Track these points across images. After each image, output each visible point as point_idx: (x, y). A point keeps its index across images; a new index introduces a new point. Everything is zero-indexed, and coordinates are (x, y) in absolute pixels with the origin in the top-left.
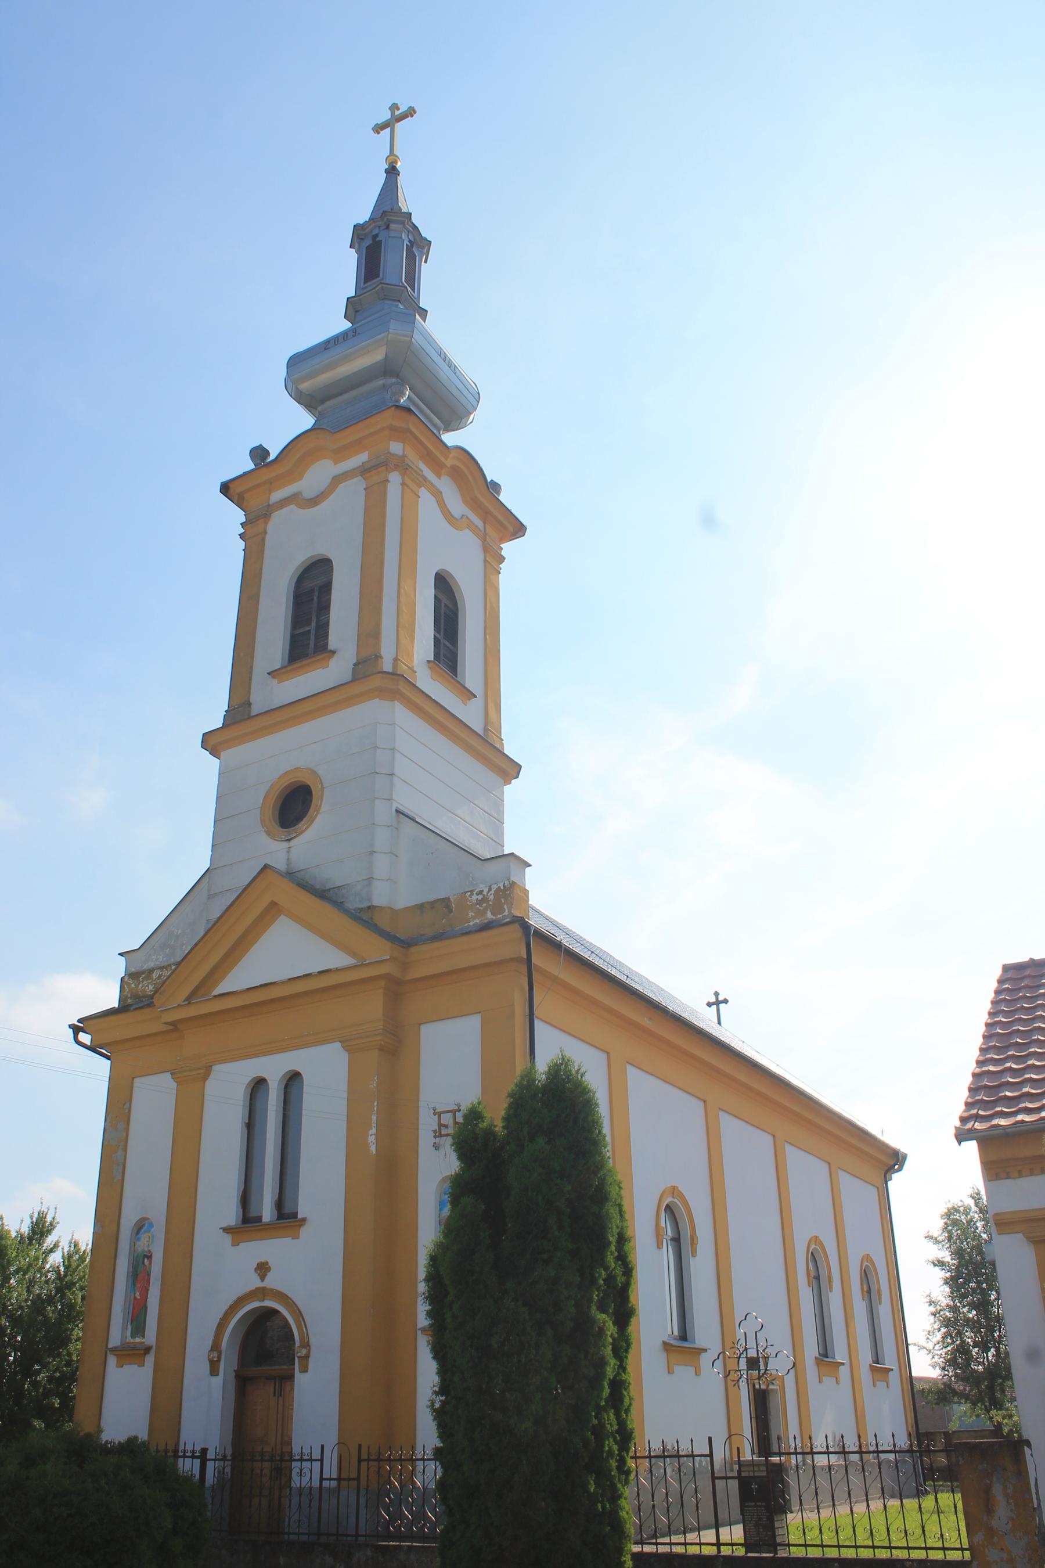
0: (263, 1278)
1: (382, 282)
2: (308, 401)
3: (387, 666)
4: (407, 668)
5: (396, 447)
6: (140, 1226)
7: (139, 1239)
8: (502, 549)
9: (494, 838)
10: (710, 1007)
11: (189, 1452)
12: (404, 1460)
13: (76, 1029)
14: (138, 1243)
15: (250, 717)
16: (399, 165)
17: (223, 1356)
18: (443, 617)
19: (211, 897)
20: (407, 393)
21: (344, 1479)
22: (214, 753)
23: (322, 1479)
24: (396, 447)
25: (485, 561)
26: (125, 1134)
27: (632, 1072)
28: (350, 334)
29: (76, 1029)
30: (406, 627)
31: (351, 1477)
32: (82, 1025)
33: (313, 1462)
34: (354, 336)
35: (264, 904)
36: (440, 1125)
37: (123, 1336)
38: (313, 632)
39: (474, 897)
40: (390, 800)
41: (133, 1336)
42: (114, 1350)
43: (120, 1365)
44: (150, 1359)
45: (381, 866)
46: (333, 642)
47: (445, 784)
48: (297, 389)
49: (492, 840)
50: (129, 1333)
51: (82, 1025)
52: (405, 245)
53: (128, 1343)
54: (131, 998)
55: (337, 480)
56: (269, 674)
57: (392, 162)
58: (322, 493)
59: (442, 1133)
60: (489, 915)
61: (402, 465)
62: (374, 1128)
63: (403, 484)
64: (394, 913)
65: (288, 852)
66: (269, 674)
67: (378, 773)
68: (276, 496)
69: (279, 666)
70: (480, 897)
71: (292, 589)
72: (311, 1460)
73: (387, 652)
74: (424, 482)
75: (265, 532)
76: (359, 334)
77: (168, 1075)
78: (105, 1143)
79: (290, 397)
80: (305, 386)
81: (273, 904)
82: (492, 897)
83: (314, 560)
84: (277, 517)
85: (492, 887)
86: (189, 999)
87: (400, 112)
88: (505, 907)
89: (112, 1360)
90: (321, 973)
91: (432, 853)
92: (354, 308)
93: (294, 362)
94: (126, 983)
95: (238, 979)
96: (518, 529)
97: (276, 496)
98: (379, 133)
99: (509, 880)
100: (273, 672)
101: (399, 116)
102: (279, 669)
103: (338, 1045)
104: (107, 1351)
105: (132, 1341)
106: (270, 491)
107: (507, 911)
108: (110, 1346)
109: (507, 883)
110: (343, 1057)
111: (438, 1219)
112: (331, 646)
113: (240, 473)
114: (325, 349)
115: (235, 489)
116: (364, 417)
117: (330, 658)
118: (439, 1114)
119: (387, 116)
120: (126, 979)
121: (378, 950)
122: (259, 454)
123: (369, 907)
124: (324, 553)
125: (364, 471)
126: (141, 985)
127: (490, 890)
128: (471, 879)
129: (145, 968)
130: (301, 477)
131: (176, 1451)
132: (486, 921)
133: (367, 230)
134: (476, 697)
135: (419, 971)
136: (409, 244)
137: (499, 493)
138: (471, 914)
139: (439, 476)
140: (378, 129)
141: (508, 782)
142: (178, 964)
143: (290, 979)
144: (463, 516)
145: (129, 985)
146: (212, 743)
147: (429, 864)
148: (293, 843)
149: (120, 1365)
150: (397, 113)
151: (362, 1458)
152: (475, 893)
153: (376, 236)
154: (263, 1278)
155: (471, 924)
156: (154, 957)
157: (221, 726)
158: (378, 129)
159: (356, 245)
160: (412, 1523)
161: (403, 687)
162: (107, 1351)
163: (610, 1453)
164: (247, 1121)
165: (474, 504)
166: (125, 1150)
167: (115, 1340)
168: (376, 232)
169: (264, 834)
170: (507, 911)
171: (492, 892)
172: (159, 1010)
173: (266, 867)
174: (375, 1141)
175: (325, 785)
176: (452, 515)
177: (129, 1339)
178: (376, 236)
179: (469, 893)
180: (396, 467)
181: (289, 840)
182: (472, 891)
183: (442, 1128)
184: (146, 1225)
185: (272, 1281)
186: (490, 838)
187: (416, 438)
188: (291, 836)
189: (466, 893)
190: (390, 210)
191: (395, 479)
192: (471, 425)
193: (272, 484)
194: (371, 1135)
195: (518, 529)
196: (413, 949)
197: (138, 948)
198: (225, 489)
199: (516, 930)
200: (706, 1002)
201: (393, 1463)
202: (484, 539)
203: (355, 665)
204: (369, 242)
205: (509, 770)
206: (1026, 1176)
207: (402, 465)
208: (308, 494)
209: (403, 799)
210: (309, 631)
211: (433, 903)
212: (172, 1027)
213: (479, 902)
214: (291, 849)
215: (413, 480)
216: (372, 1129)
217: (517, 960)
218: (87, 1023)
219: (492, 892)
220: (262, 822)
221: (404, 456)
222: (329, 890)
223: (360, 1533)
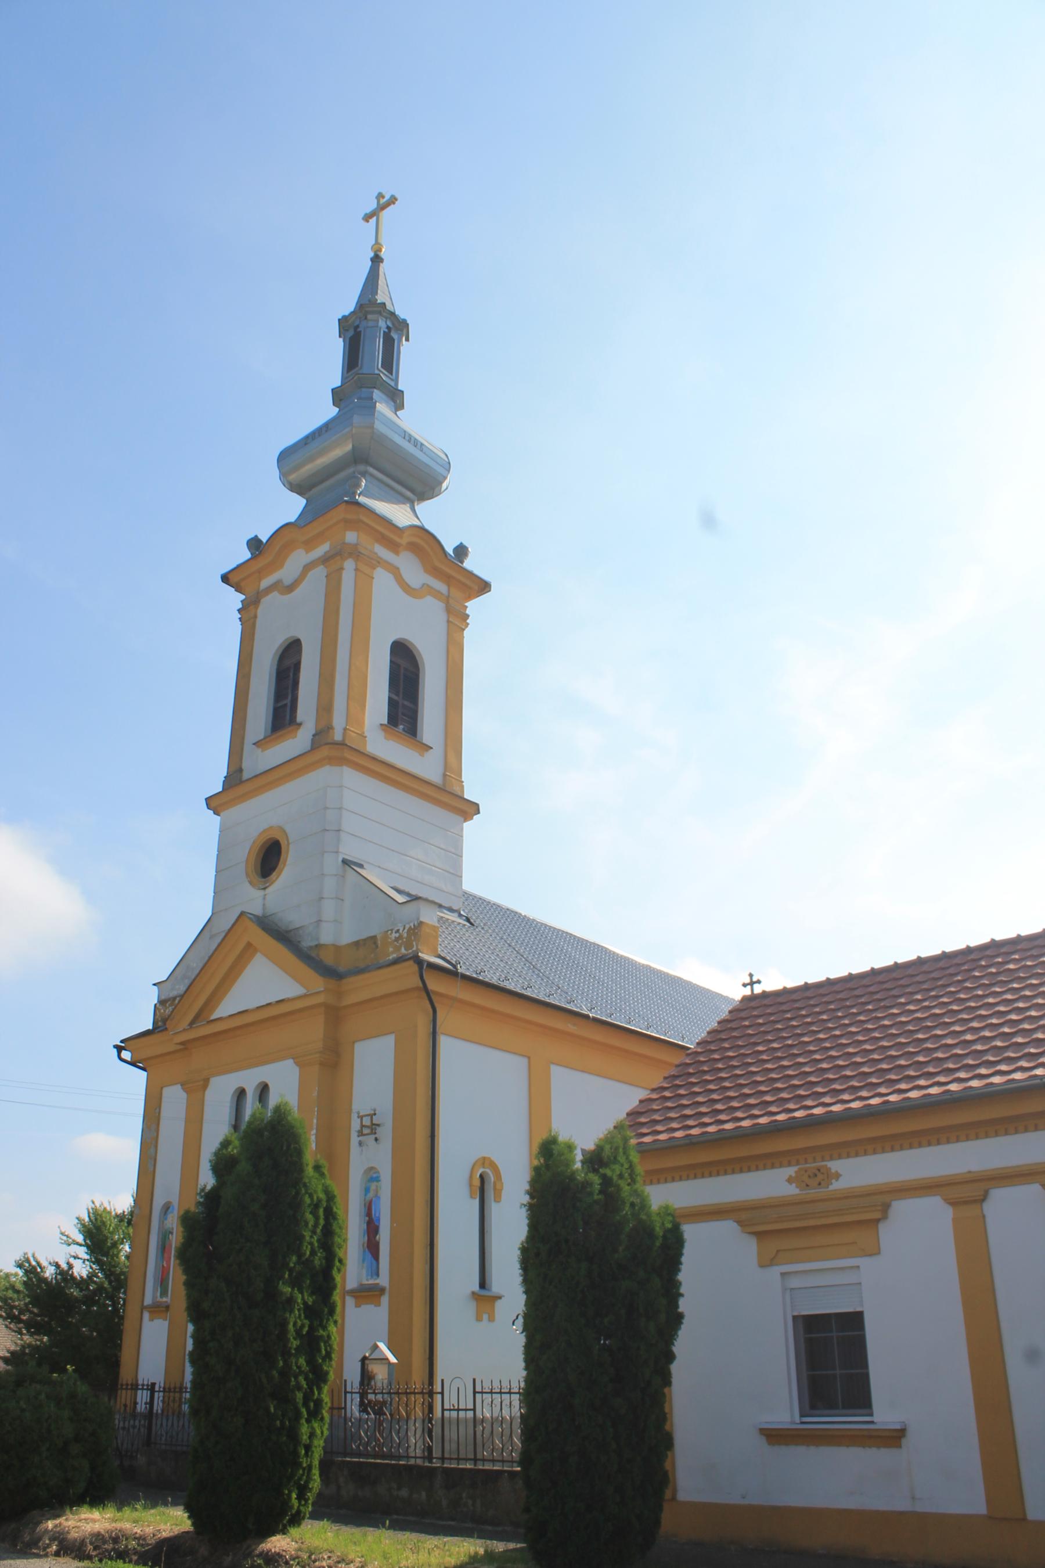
1: (360, 372)
2: (297, 488)
3: (338, 736)
4: (355, 735)
5: (351, 537)
6: (167, 1208)
7: (166, 1219)
8: (466, 607)
9: (451, 871)
12: (401, 1393)
13: (119, 1049)
14: (165, 1222)
15: (241, 782)
16: (382, 254)
18: (402, 677)
19: (212, 937)
20: (363, 484)
21: (335, 1409)
22: (216, 813)
23: (443, 1410)
24: (351, 537)
25: (448, 621)
26: (155, 1134)
27: (556, 1071)
28: (317, 435)
29: (119, 1049)
30: (358, 697)
31: (468, 1407)
32: (123, 1045)
34: (326, 431)
35: (241, 946)
36: (362, 1126)
37: (154, 1297)
38: (289, 704)
39: (394, 935)
40: (337, 852)
41: (161, 1296)
42: (147, 1307)
43: (358, 1305)
44: (385, 1300)
45: (328, 909)
46: (300, 716)
48: (288, 481)
49: (448, 872)
50: (159, 1294)
51: (123, 1045)
52: (382, 332)
53: (158, 1302)
55: (307, 568)
56: (254, 744)
57: (377, 251)
58: (295, 581)
59: (364, 1133)
60: (403, 951)
61: (354, 552)
63: (356, 570)
64: (337, 948)
65: (264, 899)
66: (254, 744)
67: (328, 830)
68: (265, 583)
69: (262, 737)
71: (275, 667)
73: (338, 722)
74: (380, 562)
75: (255, 617)
77: (179, 1086)
78: (143, 1141)
79: (283, 487)
80: (293, 477)
81: (249, 945)
82: (405, 935)
83: (290, 641)
84: (265, 601)
86: (191, 1024)
87: (385, 200)
88: (414, 943)
89: (146, 1315)
90: (278, 1002)
92: (338, 396)
93: (284, 456)
94: (158, 1008)
95: (226, 1008)
96: (484, 587)
97: (265, 583)
98: (368, 221)
99: (418, 919)
100: (258, 742)
101: (384, 203)
103: (290, 1062)
104: (143, 1308)
105: (161, 1300)
106: (260, 580)
107: (415, 947)
108: (146, 1303)
109: (416, 923)
110: (296, 1070)
111: (363, 1203)
112: (299, 719)
113: (234, 565)
114: (306, 444)
115: (234, 579)
116: (335, 506)
117: (298, 729)
119: (373, 205)
120: (158, 1005)
121: (319, 983)
123: (316, 946)
124: (293, 635)
125: (325, 560)
127: (404, 929)
128: (392, 919)
130: (282, 566)
131: (181, 1388)
132: (401, 955)
133: (350, 322)
134: (432, 748)
135: (350, 999)
136: (386, 330)
138: (391, 949)
139: (397, 553)
140: (367, 218)
141: (466, 820)
142: (182, 996)
143: (258, 1008)
144: (424, 584)
146: (214, 803)
148: (268, 890)
150: (382, 201)
151: (477, 1390)
152: (394, 931)
153: (358, 326)
155: (391, 958)
157: (221, 790)
158: (367, 218)
159: (342, 336)
160: (368, 1444)
161: (348, 755)
162: (143, 1308)
163: (299, 1387)
164: (233, 1123)
165: (435, 571)
166: (156, 1147)
167: (148, 1301)
168: (357, 323)
169: (247, 884)
170: (415, 947)
171: (406, 931)
172: (171, 1033)
173: (242, 914)
175: (290, 841)
176: (409, 586)
177: (159, 1299)
178: (358, 326)
179: (390, 932)
180: (350, 555)
181: (264, 889)
182: (392, 930)
183: (364, 1128)
186: (445, 871)
187: (367, 525)
189: (388, 931)
190: (367, 302)
191: (349, 565)
192: (446, 491)
193: (261, 573)
195: (484, 587)
196: (345, 981)
197: (165, 979)
198: (225, 579)
199: (412, 967)
201: (401, 1396)
202: (447, 600)
203: (314, 736)
204: (351, 333)
205: (469, 810)
206: (954, 1143)
207: (354, 552)
208: (287, 582)
209: (350, 850)
210: (286, 705)
211: (364, 940)
212: (181, 1047)
213: (397, 939)
214: (266, 896)
215: (368, 563)
217: (417, 989)
218: (127, 1043)
220: (247, 875)
221: (357, 545)
222: (291, 931)
223: (478, 1457)
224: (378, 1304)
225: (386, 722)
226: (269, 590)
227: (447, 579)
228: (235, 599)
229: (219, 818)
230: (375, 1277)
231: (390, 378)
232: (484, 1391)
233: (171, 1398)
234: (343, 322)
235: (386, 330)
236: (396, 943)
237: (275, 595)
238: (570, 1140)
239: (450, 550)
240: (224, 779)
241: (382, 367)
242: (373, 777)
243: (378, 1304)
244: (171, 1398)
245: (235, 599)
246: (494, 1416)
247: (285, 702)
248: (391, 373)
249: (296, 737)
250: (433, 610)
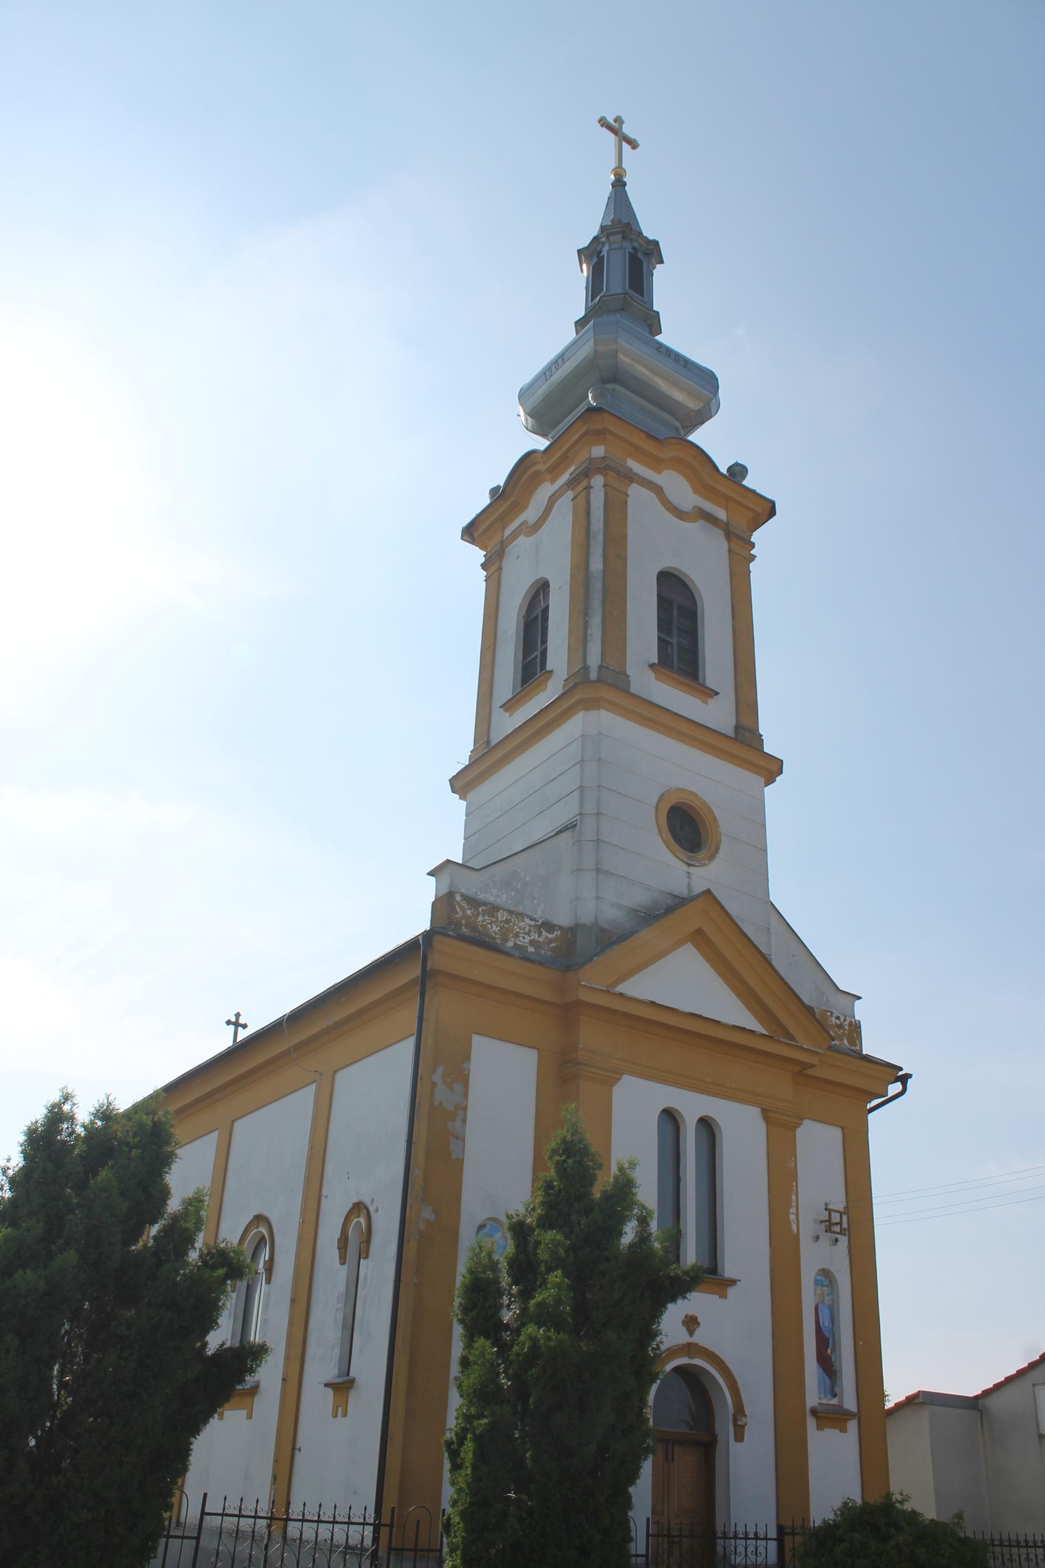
0: (691, 1333)
10: (235, 1015)
11: (799, 1528)
17: (731, 1418)
22: (463, 797)
24: (598, 451)
25: (730, 551)
33: (768, 1541)
44: (852, 1425)
47: (571, 793)
54: (466, 927)
55: (552, 500)
70: (838, 1022)
72: (766, 1539)
74: (630, 477)
76: (689, 370)
82: (847, 1027)
84: (512, 549)
85: (847, 1018)
91: (793, 956)
97: (508, 531)
102: (512, 698)
117: (549, 679)
118: (830, 1211)
122: (738, 471)
125: (571, 484)
126: (480, 918)
127: (845, 1020)
128: (826, 1000)
129: (481, 896)
130: (659, 471)
136: (632, 251)
137: (498, 487)
145: (463, 909)
147: (790, 964)
149: (819, 1428)
154: (691, 1333)
156: (494, 891)
171: (847, 1022)
181: (690, 865)
184: (488, 1227)
185: (700, 1337)
188: (693, 863)
189: (827, 1011)
197: (841, 989)
200: (241, 1013)
208: (531, 522)
219: (847, 1022)
224: (844, 1430)
225: (656, 661)
226: (516, 534)
227: (725, 501)
228: (478, 555)
229: (465, 803)
230: (829, 1396)
231: (642, 301)
232: (227, 1511)
233: (1024, 1556)
234: (584, 254)
235: (632, 251)
236: (837, 1029)
237: (522, 539)
238: (596, 920)
239: (723, 470)
240: (470, 754)
241: (630, 288)
242: (658, 731)
243: (844, 1430)
244: (1024, 1556)
245: (478, 555)
246: (758, 1563)
247: (534, 655)
248: (642, 295)
249: (546, 688)
250: (717, 544)
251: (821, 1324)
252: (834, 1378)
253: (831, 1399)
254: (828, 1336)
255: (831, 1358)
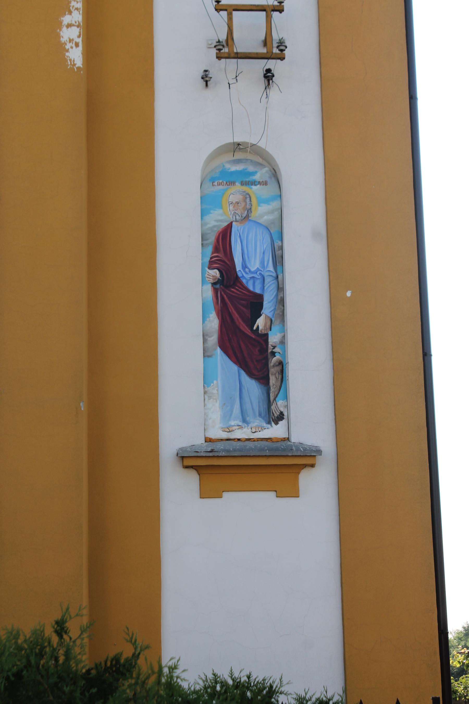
62: (75, 13)
174: (80, 40)
194: (69, 26)
216: (70, 13)
230: (259, 422)
251: (239, 267)
252: (273, 380)
253: (263, 428)
254: (258, 291)
255: (266, 336)
